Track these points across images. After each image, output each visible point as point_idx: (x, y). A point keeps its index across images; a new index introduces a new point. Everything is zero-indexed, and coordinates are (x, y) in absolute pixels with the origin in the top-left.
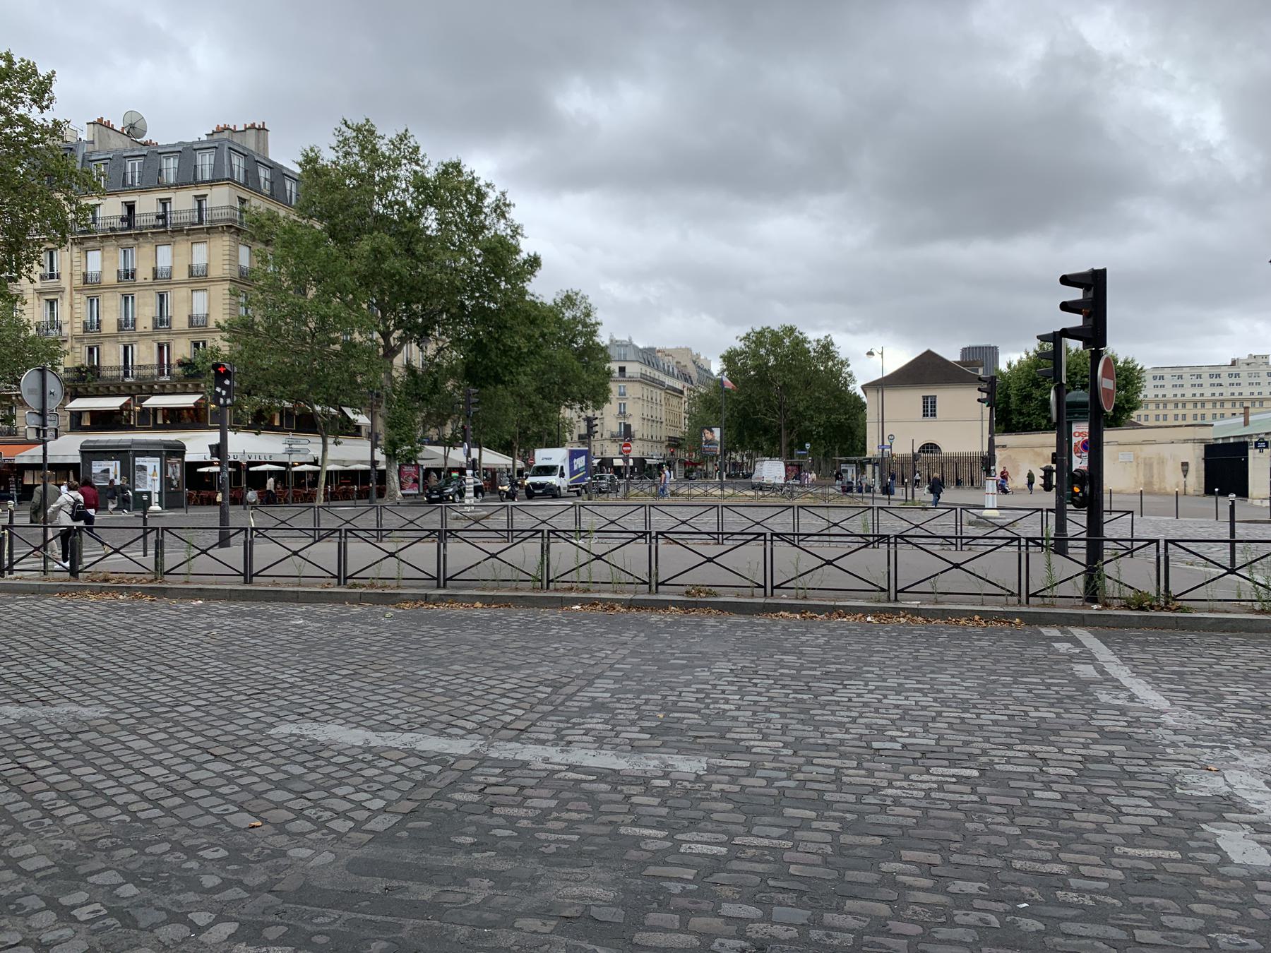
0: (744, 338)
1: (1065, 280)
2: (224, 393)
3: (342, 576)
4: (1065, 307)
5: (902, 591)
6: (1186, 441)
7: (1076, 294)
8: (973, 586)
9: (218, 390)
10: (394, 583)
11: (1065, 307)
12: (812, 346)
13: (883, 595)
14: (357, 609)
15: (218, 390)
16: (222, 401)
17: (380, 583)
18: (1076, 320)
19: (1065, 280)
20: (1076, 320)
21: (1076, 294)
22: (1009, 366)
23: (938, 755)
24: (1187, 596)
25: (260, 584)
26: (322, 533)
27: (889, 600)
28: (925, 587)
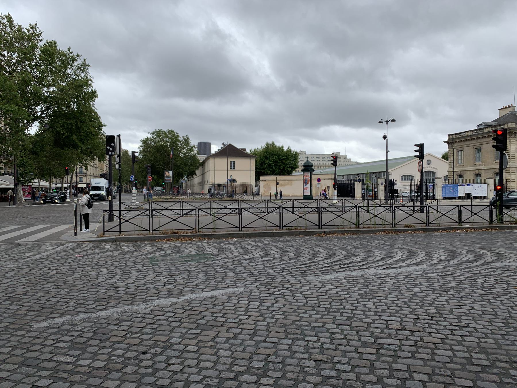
0: (152, 133)
1: (415, 145)
2: (111, 149)
3: (320, 225)
4: (415, 151)
5: (244, 227)
6: (329, 179)
7: (418, 148)
8: (480, 220)
9: (108, 148)
10: (304, 228)
11: (415, 151)
12: (181, 139)
13: (238, 229)
14: (356, 236)
15: (108, 148)
16: (110, 153)
17: (299, 228)
18: (418, 154)
19: (415, 145)
20: (418, 154)
21: (418, 148)
22: (251, 151)
23: (265, 292)
24: (364, 223)
25: (431, 226)
26: (269, 210)
27: (239, 231)
28: (435, 222)
